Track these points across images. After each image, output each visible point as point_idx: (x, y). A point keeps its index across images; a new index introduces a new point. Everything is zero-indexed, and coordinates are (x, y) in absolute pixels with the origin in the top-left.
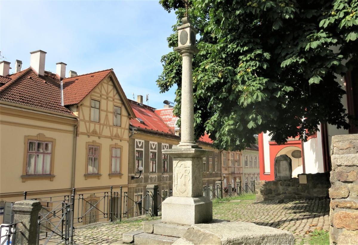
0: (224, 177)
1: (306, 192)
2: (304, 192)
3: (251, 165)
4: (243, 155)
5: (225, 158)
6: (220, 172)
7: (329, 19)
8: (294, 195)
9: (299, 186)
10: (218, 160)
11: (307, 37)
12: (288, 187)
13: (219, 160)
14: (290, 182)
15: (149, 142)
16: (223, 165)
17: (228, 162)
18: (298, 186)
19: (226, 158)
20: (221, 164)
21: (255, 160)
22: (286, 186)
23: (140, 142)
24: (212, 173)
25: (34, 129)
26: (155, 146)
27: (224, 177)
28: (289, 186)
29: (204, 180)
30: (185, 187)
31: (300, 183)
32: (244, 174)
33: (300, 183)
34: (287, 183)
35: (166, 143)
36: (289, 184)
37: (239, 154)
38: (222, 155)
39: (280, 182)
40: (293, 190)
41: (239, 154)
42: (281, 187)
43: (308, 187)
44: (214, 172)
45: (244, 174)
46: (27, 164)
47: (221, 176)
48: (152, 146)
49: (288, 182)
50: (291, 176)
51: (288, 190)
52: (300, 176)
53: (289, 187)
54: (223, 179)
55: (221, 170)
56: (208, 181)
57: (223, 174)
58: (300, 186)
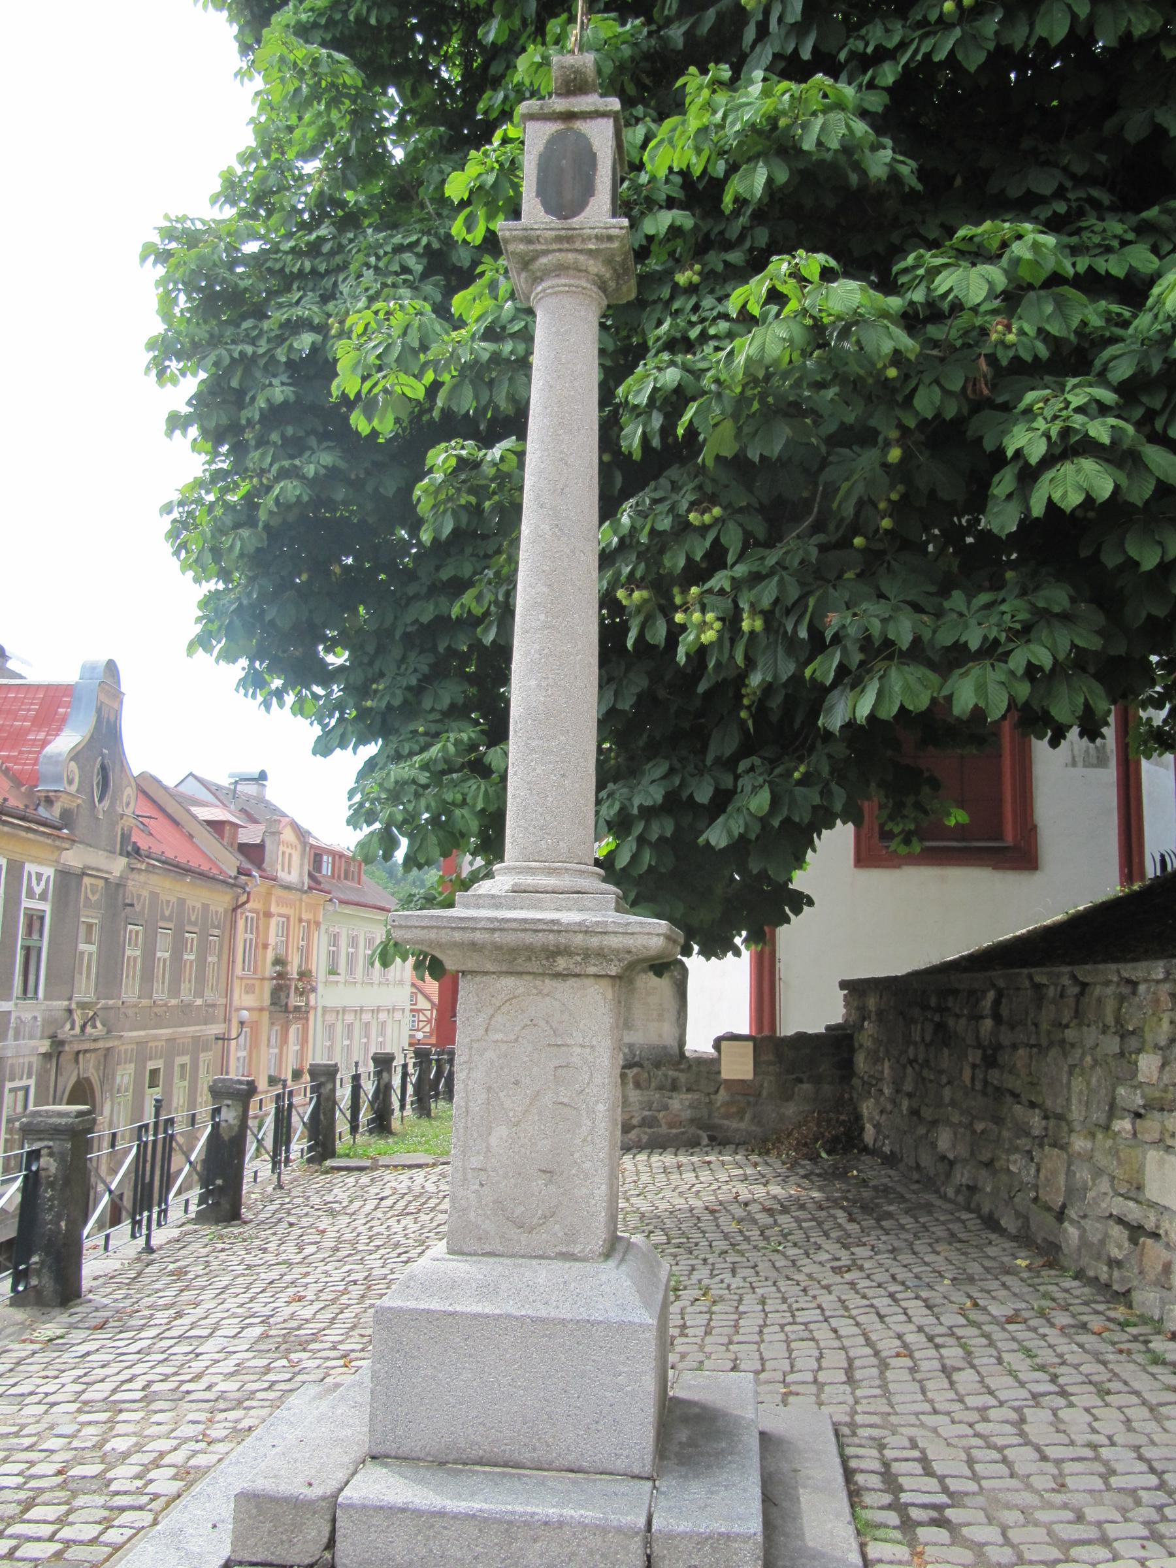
0: (242, 1023)
1: (748, 1116)
2: (741, 1114)
3: (351, 971)
4: (323, 928)
5: (249, 936)
6: (223, 1001)
7: (437, 605)
8: (693, 1130)
9: (717, 1092)
10: (221, 946)
11: (630, 644)
12: (668, 1094)
13: (226, 947)
14: (676, 1074)
15: (21, 866)
16: (239, 971)
17: (260, 958)
18: (712, 1090)
19: (253, 936)
20: (231, 962)
21: (351, 950)
22: (660, 1088)
23: (39, 876)
24: (189, 1005)
25: (247, 865)
26: (43, 883)
27: (242, 1023)
28: (674, 1087)
29: (156, 1038)
30: (552, 1188)
31: (725, 1075)
32: (320, 1010)
33: (725, 1075)
34: (666, 1076)
35: (40, 862)
36: (674, 1080)
37: (309, 922)
38: (241, 924)
39: (635, 1070)
40: (691, 1106)
41: (309, 922)
42: (638, 1092)
43: (759, 1095)
44: (199, 1002)
45: (320, 1010)
46: (502, 1464)
47: (227, 1020)
48: (34, 881)
49: (670, 1073)
50: (682, 1042)
51: (666, 1108)
52: (724, 1044)
53: (674, 1095)
54: (234, 1035)
55: (228, 992)
56: (171, 1041)
57: (238, 1010)
58: (722, 1091)
